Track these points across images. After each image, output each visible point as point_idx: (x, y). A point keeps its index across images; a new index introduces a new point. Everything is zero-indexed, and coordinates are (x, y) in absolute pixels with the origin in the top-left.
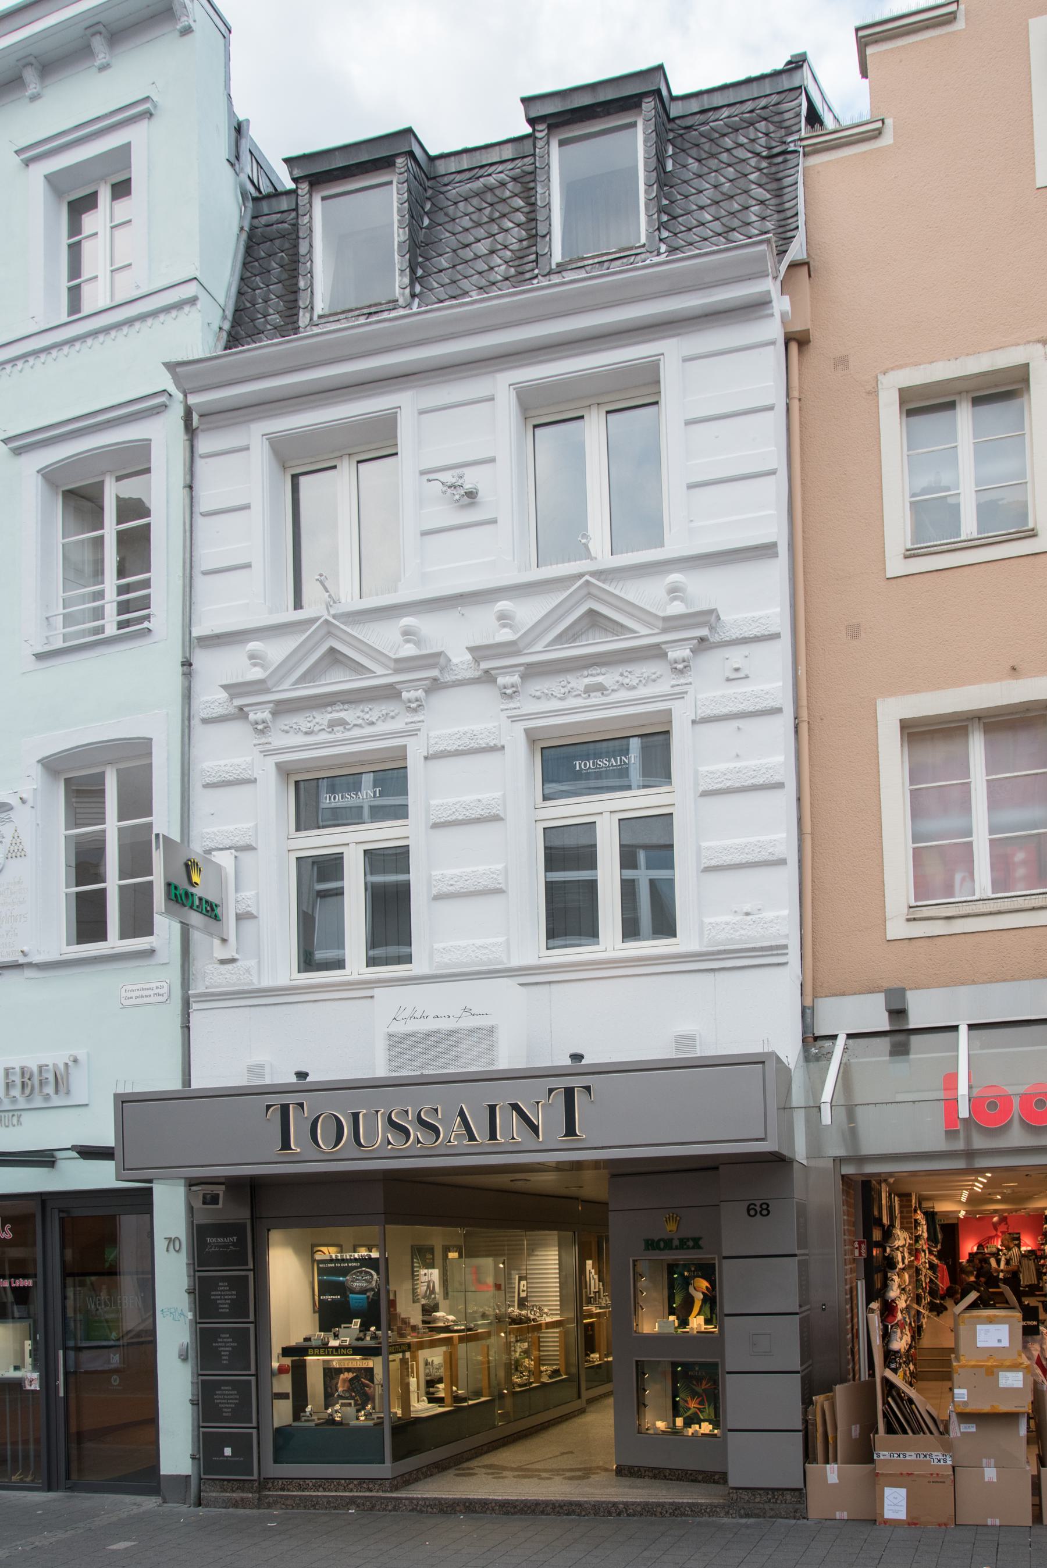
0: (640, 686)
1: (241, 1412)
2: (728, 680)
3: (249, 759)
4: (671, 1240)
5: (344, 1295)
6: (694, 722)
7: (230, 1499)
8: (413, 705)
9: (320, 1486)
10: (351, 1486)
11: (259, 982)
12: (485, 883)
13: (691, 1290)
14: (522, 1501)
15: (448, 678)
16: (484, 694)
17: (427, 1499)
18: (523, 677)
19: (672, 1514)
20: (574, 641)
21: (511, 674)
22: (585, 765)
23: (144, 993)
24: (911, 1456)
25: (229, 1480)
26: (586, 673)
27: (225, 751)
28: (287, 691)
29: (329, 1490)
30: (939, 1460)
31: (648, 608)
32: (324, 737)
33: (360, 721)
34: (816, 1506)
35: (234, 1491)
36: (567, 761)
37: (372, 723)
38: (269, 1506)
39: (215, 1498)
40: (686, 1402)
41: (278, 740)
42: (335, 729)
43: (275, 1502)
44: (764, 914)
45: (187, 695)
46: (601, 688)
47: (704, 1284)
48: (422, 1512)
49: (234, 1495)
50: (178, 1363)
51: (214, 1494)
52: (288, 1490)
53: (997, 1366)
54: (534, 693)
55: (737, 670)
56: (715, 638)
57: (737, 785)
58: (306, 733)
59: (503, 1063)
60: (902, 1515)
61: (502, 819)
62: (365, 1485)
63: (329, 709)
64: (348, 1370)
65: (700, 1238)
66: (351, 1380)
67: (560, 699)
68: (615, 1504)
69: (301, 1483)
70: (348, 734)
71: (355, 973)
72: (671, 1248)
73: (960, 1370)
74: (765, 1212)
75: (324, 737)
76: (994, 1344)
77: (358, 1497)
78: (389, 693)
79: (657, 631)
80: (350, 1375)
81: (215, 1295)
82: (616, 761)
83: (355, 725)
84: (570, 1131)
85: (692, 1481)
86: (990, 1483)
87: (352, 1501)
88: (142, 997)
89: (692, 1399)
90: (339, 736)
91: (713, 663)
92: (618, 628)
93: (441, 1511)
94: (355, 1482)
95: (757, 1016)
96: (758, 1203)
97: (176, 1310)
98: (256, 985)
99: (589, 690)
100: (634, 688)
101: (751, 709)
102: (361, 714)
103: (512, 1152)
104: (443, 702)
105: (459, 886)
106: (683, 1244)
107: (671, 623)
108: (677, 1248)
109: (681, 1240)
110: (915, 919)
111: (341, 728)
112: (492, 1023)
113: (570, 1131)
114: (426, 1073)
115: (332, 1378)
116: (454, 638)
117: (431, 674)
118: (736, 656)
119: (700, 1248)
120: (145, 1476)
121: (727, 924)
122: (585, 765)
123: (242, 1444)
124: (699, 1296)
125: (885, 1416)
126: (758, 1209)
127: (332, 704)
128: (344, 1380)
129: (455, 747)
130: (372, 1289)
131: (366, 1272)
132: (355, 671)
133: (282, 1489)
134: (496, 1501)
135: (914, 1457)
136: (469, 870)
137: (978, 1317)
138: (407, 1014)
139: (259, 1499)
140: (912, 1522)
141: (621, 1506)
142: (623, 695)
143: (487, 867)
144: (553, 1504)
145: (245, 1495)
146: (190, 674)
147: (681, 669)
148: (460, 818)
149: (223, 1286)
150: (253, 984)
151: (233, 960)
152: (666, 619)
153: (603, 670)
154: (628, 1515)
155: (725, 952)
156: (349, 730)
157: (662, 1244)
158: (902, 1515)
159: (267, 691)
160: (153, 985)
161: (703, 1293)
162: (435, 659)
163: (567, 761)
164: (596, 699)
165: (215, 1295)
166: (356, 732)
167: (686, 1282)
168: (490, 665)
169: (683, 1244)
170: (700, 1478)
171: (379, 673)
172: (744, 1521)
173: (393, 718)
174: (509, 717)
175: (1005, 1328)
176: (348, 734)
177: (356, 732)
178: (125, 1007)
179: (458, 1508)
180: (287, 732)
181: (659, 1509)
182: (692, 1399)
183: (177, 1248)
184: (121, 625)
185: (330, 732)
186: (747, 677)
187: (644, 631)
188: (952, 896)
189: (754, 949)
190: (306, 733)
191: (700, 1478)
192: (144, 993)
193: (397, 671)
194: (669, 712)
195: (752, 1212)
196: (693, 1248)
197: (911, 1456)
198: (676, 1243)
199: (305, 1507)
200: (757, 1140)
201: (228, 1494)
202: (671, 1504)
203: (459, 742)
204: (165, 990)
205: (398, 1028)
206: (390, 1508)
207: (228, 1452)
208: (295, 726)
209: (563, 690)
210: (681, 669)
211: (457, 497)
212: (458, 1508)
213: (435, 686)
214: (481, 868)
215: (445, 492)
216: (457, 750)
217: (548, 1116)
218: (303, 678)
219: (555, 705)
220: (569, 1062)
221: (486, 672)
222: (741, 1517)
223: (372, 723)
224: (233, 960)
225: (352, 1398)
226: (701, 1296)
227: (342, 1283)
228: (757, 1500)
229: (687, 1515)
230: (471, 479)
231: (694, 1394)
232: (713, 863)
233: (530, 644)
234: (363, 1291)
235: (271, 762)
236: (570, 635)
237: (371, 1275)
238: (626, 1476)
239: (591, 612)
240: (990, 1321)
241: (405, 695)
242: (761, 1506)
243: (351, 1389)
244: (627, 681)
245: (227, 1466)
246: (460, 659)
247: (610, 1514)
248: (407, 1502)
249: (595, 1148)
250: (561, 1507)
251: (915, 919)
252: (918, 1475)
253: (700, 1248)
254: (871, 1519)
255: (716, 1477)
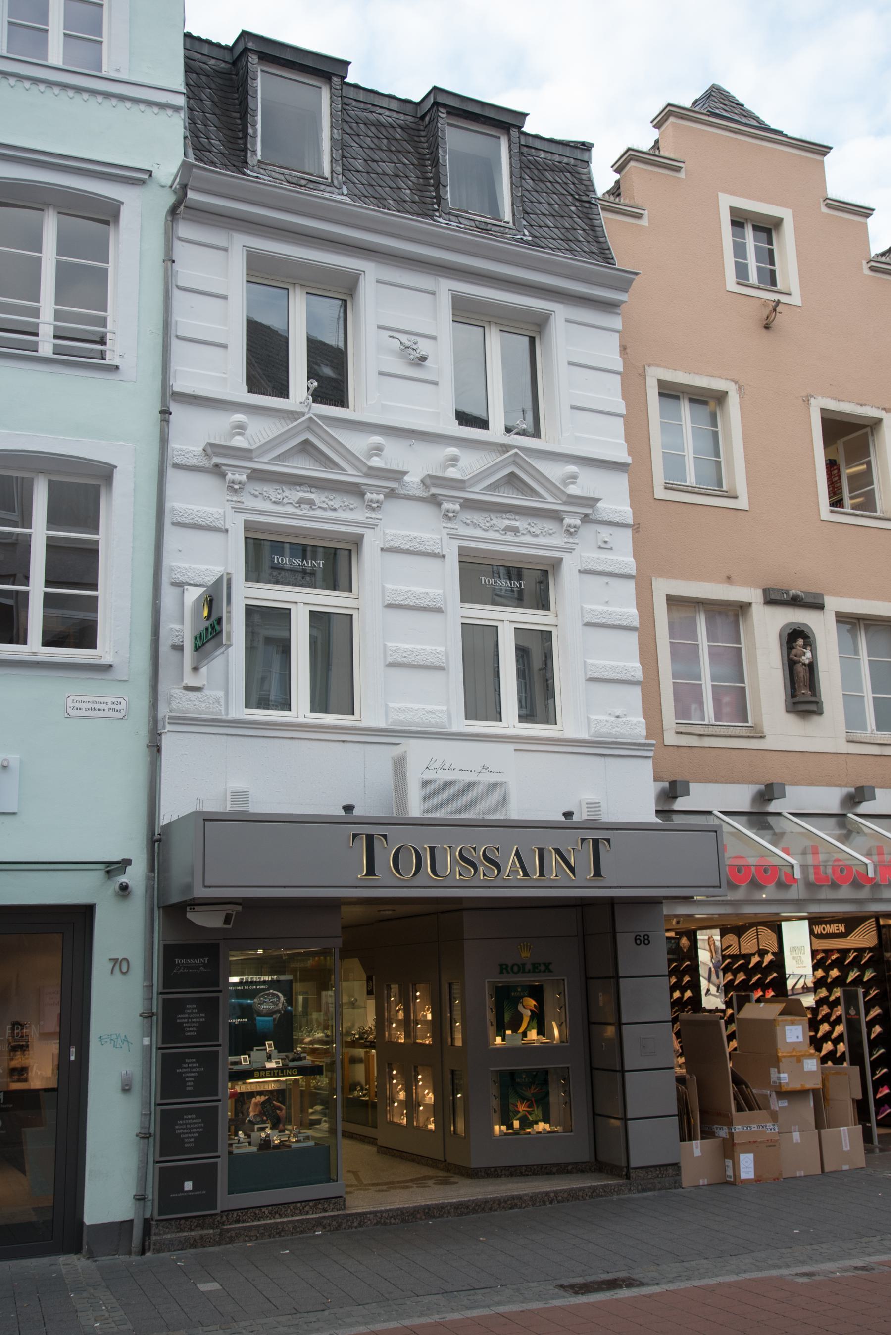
0: (541, 536)
1: (208, 1141)
2: (600, 547)
3: (436, 537)
4: (524, 965)
5: (252, 1019)
6: (382, 549)
7: (187, 1239)
8: (375, 505)
9: (276, 1213)
10: (307, 1208)
11: (227, 713)
12: (431, 660)
13: (520, 1008)
14: (473, 1201)
15: (402, 492)
16: (426, 512)
17: (390, 1210)
18: (249, 477)
19: (591, 1197)
20: (494, 490)
21: (454, 503)
22: (282, 560)
23: (97, 706)
24: (755, 1128)
25: (186, 1218)
26: (504, 516)
27: (193, 498)
28: (265, 464)
29: (286, 1216)
30: (771, 1129)
31: (353, 451)
32: (290, 509)
33: (325, 506)
34: (687, 1179)
35: (191, 1230)
36: (266, 554)
37: (335, 509)
38: (231, 1240)
39: (170, 1240)
40: (516, 1106)
41: (250, 503)
42: (303, 506)
43: (238, 1236)
44: (628, 719)
45: (164, 440)
46: (311, 503)
47: (532, 1003)
48: (385, 1224)
49: (193, 1234)
50: (118, 1096)
51: (169, 1236)
52: (244, 1221)
53: (802, 1056)
54: (465, 521)
55: (606, 542)
56: (592, 517)
57: (609, 623)
58: (275, 502)
59: (515, 814)
60: (751, 1175)
61: (442, 612)
62: (320, 1206)
63: (298, 488)
64: (260, 1093)
65: (550, 963)
66: (263, 1104)
67: (484, 530)
68: (547, 1194)
69: (256, 1211)
70: (312, 513)
71: (301, 715)
72: (524, 972)
73: (783, 1059)
74: (646, 942)
75: (290, 509)
76: (794, 1040)
77: (324, 1217)
78: (356, 491)
79: (559, 502)
80: (262, 1099)
81: (181, 1018)
82: (308, 563)
83: (320, 507)
84: (598, 873)
85: (547, 1174)
86: (797, 1143)
87: (319, 1223)
88: (94, 709)
89: (521, 1104)
90: (305, 512)
91: (588, 533)
92: (327, 462)
93: (403, 1220)
94: (311, 1204)
95: (627, 795)
96: (642, 934)
97: (118, 1036)
98: (223, 716)
99: (507, 529)
100: (537, 536)
101: (616, 572)
102: (326, 500)
103: (551, 887)
104: (393, 508)
105: (411, 659)
106: (535, 968)
107: (373, 472)
108: (529, 972)
109: (533, 964)
110: (681, 733)
111: (308, 506)
112: (504, 780)
113: (598, 873)
114: (486, 817)
115: (243, 1103)
116: (416, 464)
117: (391, 483)
118: (605, 533)
119: (550, 971)
120: (60, 1226)
121: (607, 722)
122: (282, 560)
123: (205, 1177)
124: (527, 1013)
125: (735, 1099)
126: (642, 939)
127: (300, 485)
128: (256, 1104)
129: (407, 547)
130: (278, 1011)
131: (273, 995)
132: (317, 460)
133: (238, 1221)
134: (451, 1204)
135: (756, 1129)
136: (419, 647)
137: (786, 1020)
138: (437, 765)
139: (221, 1235)
140: (758, 1180)
141: (552, 1195)
142: (528, 539)
143: (433, 648)
144: (499, 1200)
145: (205, 1232)
146: (168, 422)
147: (571, 532)
148: (411, 604)
149: (191, 1008)
150: (220, 714)
151: (198, 689)
152: (570, 496)
153: (517, 518)
154: (558, 1202)
155: (616, 743)
156: (314, 509)
157: (516, 969)
158: (751, 1175)
159: (250, 459)
160: (110, 700)
161: (531, 1010)
162: (398, 475)
163: (266, 554)
164: (510, 537)
165: (181, 1018)
166: (319, 513)
167: (518, 1000)
168: (436, 493)
169: (535, 968)
170: (554, 1170)
171: (350, 473)
172: (640, 1195)
173: (352, 509)
174: (448, 534)
175: (800, 1028)
176: (312, 513)
177: (319, 513)
178: (71, 717)
179: (418, 1216)
180: (256, 496)
181: (581, 1194)
182: (521, 1104)
183: (124, 970)
184: (57, 350)
185: (296, 507)
186: (611, 549)
187: (550, 499)
188: (690, 720)
189: (634, 744)
190: (275, 502)
191: (554, 1170)
192: (97, 706)
193: (366, 475)
194: (363, 536)
195: (638, 942)
196: (544, 971)
197: (755, 1128)
198: (529, 967)
199: (270, 1236)
200: (714, 887)
201: (185, 1234)
202: (589, 1188)
203: (410, 544)
204: (123, 706)
205: (431, 776)
206: (356, 1224)
207: (188, 1186)
208: (265, 494)
209: (487, 524)
210: (571, 532)
211: (412, 357)
212: (418, 1216)
213: (391, 494)
214: (428, 648)
215: (403, 350)
216: (408, 549)
217: (583, 859)
218: (279, 458)
219: (479, 533)
220: (342, 812)
221: (217, 466)
222: (639, 1192)
223: (335, 509)
224: (198, 689)
225: (264, 1122)
226: (529, 1013)
227: (250, 1006)
228: (650, 1176)
229: (602, 1196)
230: (424, 347)
231: (523, 1099)
232: (596, 675)
233: (471, 486)
234: (270, 1013)
235: (240, 519)
236: (494, 487)
237: (278, 997)
238: (483, 1177)
239: (307, 442)
240: (793, 1023)
241: (368, 496)
242: (652, 1181)
243: (262, 1113)
244: (532, 530)
245: (189, 1202)
246: (413, 479)
247: (544, 1203)
248: (371, 1216)
249: (611, 887)
250: (505, 1202)
251: (681, 733)
252: (761, 1142)
253: (550, 971)
254: (729, 1183)
255: (570, 1168)
